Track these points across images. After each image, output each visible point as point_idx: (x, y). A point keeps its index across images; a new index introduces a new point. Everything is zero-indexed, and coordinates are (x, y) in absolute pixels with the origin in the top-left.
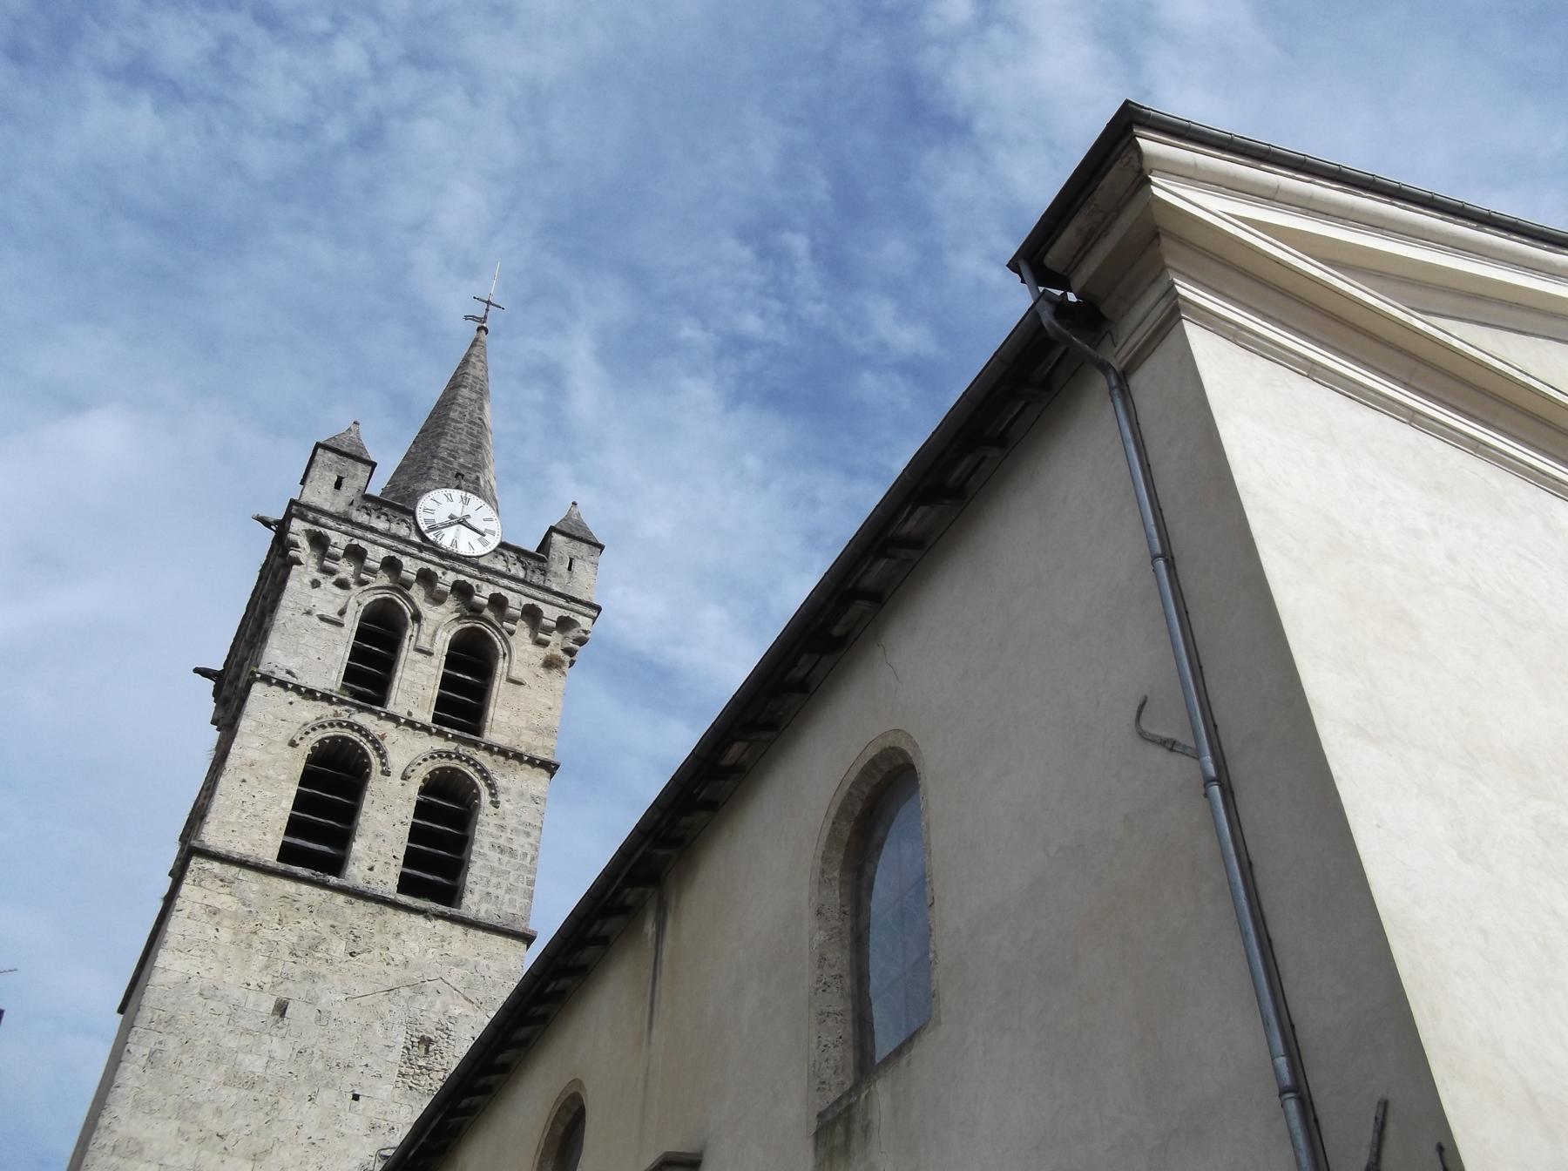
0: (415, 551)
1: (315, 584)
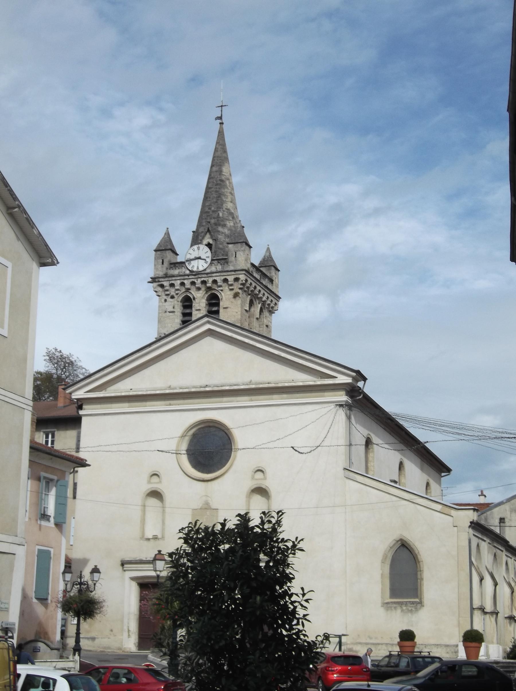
0: (187, 277)
1: (166, 301)
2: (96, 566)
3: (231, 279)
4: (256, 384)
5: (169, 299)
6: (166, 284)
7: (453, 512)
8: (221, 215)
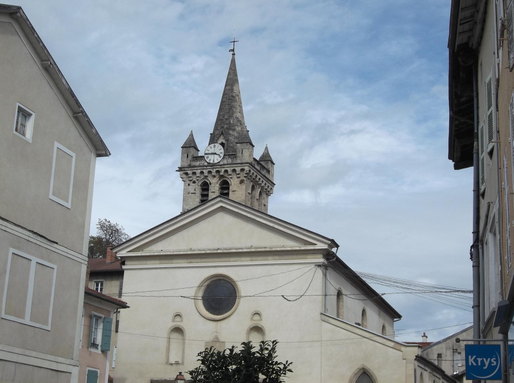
1: (189, 185)
3: (238, 169)
5: (191, 184)
6: (190, 172)
8: (232, 122)
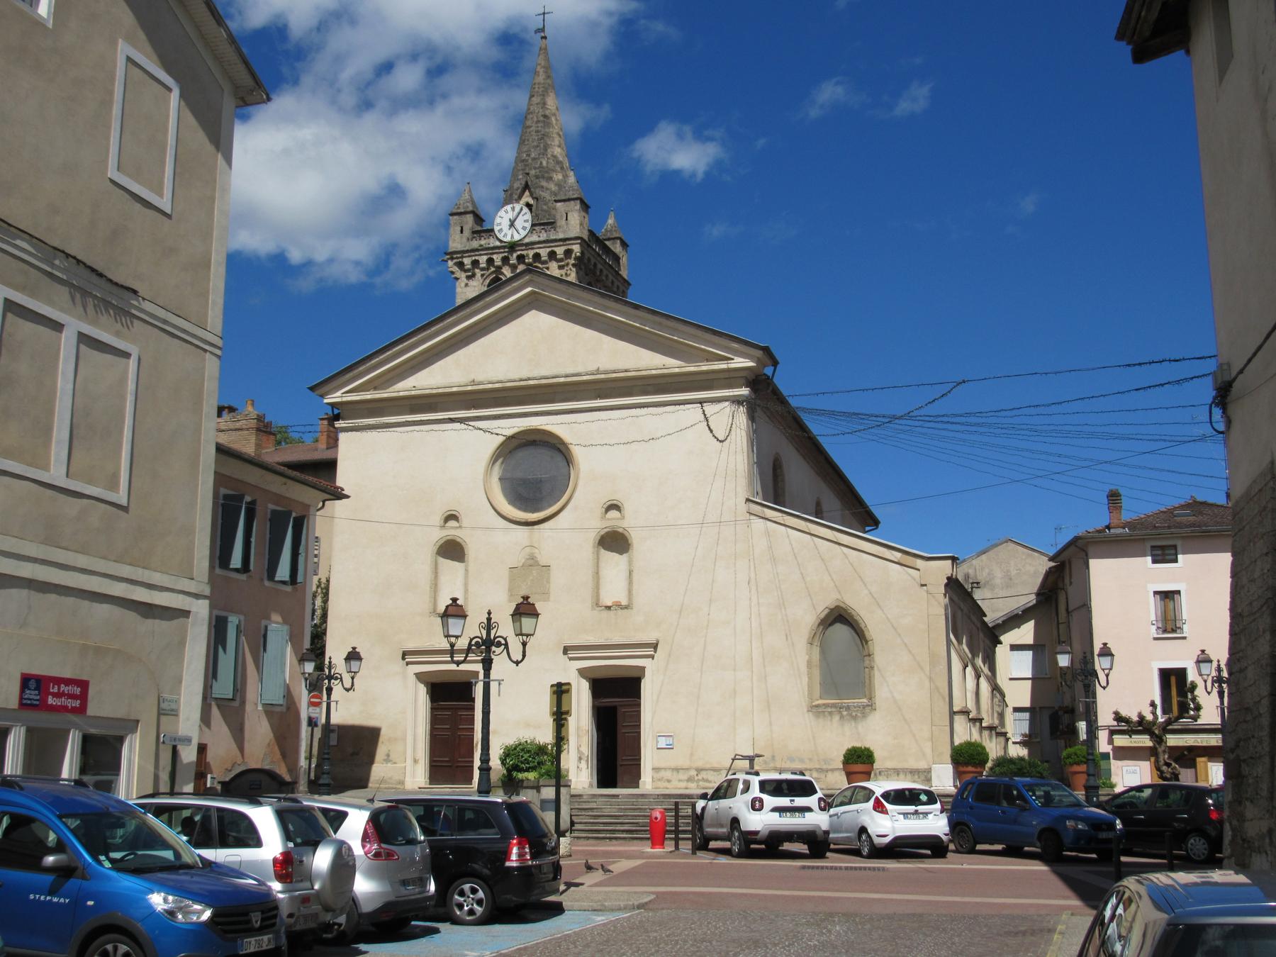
2: (354, 648)
3: (560, 251)
4: (606, 372)
7: (920, 563)
8: (544, 163)
